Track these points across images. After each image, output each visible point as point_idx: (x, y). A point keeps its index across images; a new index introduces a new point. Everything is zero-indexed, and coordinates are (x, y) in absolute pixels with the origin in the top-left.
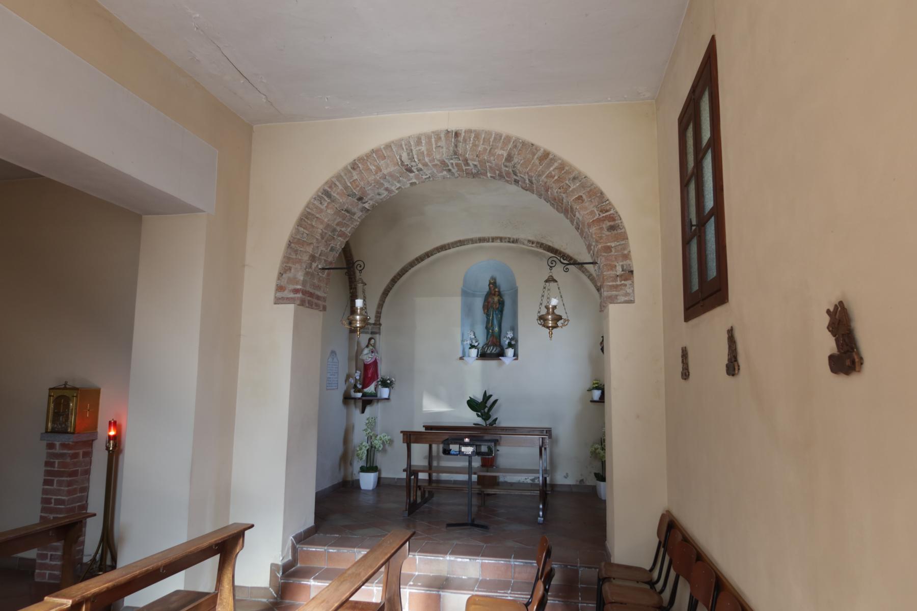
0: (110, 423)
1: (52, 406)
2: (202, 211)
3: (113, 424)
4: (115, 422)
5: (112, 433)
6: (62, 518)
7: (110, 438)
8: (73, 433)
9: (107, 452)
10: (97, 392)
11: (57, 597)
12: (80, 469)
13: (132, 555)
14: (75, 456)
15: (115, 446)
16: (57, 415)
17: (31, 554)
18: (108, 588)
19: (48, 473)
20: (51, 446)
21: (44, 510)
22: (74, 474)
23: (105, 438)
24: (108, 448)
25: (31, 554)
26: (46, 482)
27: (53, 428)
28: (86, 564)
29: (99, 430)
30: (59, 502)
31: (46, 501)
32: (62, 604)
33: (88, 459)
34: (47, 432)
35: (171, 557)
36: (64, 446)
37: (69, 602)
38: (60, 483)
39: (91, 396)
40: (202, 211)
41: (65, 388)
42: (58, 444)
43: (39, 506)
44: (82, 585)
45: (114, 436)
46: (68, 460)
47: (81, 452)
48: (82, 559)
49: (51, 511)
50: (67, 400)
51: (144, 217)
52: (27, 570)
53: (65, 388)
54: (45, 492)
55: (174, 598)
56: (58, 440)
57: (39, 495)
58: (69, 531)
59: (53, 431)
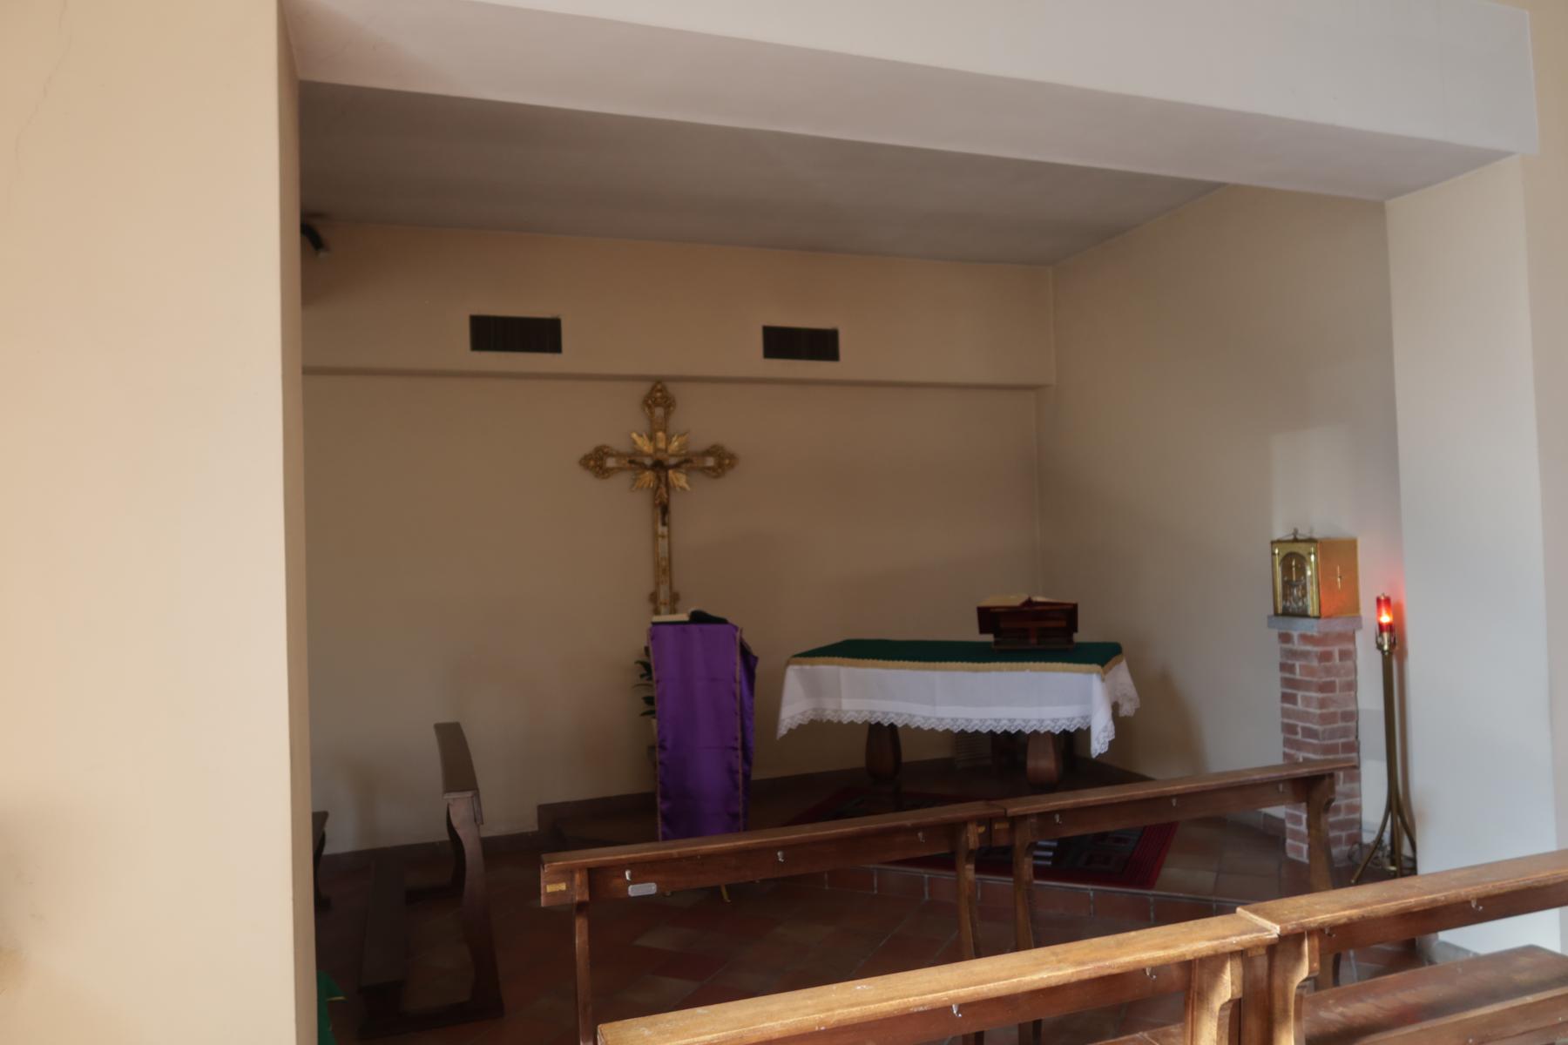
0: (1379, 600)
1: (1279, 569)
2: (1508, 154)
3: (1384, 602)
4: (1388, 601)
5: (1386, 619)
6: (1310, 758)
7: (1381, 627)
8: (1318, 618)
9: (1378, 654)
10: (1350, 546)
11: (1255, 912)
12: (1337, 680)
13: (1448, 855)
14: (1326, 657)
15: (1392, 645)
16: (1288, 585)
17: (1279, 811)
18: (1350, 918)
19: (1288, 683)
20: (1285, 638)
21: (1288, 743)
22: (1327, 687)
23: (1374, 629)
24: (1380, 647)
25: (1279, 811)
26: (1287, 698)
27: (1285, 608)
28: (1368, 846)
29: (1363, 612)
30: (1309, 733)
31: (1289, 729)
32: (1263, 930)
33: (1349, 663)
34: (1276, 614)
35: (1491, 885)
36: (1305, 638)
37: (1274, 930)
38: (1307, 701)
39: (1340, 553)
40: (1508, 154)
41: (1296, 540)
42: (1295, 634)
43: (1279, 737)
44: (1303, 900)
45: (1390, 628)
46: (1315, 663)
47: (1336, 650)
48: (1359, 835)
49: (1298, 745)
50: (1302, 561)
51: (1389, 204)
52: (1273, 836)
53: (1296, 540)
54: (1285, 713)
55: (1524, 961)
56: (1299, 627)
57: (1278, 720)
58: (1313, 788)
59: (1287, 613)
